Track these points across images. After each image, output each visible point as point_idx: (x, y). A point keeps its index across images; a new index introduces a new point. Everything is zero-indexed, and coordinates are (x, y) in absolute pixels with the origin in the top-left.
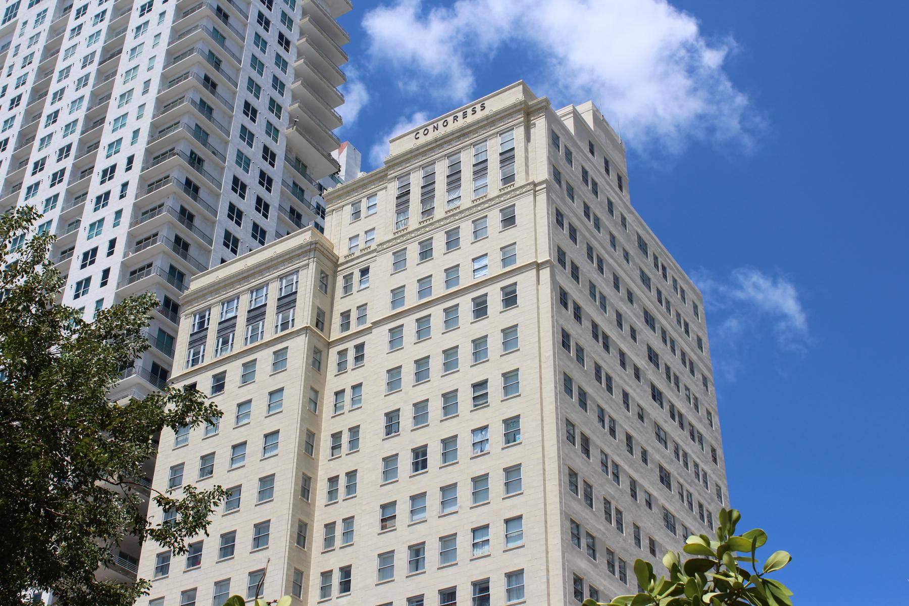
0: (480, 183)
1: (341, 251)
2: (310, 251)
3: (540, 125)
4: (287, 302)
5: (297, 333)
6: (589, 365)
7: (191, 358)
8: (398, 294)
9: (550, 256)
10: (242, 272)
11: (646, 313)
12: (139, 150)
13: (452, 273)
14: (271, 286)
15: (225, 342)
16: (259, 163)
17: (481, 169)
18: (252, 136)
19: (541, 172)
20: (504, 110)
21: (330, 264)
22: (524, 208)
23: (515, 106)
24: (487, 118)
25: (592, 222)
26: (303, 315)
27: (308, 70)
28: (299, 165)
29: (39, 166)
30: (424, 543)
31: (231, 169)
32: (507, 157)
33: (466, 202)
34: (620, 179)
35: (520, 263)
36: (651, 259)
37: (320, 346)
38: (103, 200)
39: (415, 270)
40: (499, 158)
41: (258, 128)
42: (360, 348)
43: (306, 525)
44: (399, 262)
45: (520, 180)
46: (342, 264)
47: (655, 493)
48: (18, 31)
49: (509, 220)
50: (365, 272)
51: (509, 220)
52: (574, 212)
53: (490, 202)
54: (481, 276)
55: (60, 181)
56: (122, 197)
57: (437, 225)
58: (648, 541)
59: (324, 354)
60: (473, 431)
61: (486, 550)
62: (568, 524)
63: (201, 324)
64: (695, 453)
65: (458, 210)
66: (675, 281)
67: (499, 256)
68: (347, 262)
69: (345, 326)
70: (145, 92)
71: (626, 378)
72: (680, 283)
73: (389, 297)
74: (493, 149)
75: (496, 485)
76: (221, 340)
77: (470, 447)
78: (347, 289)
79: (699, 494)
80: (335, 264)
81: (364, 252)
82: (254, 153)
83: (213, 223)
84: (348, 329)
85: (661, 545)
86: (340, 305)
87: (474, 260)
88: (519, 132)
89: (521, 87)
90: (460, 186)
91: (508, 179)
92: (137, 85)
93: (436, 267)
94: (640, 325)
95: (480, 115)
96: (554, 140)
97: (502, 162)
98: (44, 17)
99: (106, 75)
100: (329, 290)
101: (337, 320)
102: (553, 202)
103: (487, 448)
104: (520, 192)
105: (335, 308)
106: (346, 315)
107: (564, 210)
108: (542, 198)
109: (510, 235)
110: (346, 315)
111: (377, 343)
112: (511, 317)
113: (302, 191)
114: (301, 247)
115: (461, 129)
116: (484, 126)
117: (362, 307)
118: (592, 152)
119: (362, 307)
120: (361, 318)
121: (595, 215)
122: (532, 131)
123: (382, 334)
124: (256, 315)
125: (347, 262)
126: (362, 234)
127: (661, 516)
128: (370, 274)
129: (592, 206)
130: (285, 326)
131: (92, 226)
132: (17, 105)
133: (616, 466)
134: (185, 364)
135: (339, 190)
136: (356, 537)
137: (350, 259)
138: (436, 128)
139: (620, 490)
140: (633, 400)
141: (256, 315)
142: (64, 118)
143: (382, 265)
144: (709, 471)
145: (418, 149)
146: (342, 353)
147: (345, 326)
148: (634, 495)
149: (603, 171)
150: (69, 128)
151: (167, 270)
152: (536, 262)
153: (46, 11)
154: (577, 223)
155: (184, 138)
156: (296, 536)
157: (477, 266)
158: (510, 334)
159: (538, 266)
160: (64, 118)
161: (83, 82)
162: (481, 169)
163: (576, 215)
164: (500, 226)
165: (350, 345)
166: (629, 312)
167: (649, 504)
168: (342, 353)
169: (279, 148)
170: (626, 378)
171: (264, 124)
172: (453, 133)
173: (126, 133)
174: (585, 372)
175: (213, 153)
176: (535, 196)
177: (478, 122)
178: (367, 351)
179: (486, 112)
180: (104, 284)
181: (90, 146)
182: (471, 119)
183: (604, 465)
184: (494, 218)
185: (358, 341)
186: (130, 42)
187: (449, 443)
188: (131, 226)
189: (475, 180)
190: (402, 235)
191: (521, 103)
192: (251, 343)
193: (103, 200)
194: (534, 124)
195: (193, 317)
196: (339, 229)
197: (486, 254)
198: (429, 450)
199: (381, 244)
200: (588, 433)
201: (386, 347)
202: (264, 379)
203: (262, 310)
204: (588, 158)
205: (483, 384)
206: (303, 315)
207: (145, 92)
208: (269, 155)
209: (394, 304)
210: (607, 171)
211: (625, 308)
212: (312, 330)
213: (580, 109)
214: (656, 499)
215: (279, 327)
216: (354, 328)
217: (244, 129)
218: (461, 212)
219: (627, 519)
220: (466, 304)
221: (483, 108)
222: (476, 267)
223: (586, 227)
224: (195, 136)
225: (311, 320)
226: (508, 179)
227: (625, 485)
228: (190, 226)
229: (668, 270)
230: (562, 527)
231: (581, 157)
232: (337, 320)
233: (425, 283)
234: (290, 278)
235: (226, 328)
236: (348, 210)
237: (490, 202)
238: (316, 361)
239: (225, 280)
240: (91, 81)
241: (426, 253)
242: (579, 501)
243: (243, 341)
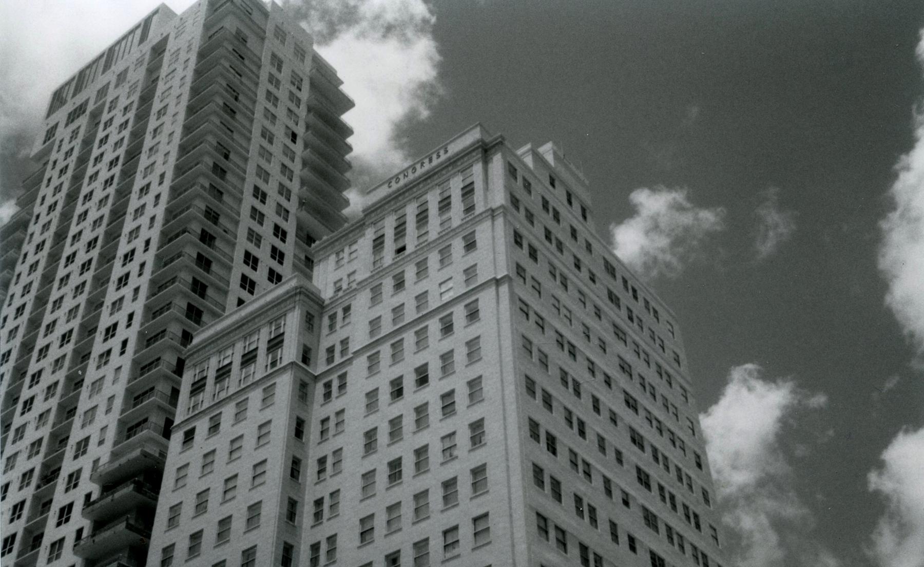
0: (445, 217)
1: (327, 294)
2: (296, 294)
3: (497, 163)
4: (276, 343)
5: (284, 368)
6: (554, 371)
8: (375, 324)
9: (508, 270)
10: (237, 322)
11: (615, 326)
12: (155, 234)
16: (269, 239)
17: (445, 205)
18: (262, 215)
19: (499, 198)
21: (316, 307)
22: (483, 233)
23: (471, 145)
24: (449, 159)
25: (554, 245)
26: (290, 352)
27: (315, 158)
29: (71, 259)
30: (399, 551)
31: (243, 244)
32: (468, 191)
33: (433, 235)
34: (584, 210)
35: (481, 280)
36: (619, 281)
37: (307, 379)
38: (123, 280)
39: (389, 300)
41: (268, 209)
42: (343, 377)
43: (292, 547)
44: (376, 293)
45: (480, 209)
46: (328, 305)
47: (632, 492)
48: (56, 148)
49: (470, 245)
50: (347, 310)
51: (470, 245)
52: (534, 235)
53: (454, 232)
54: (446, 298)
55: (88, 269)
56: (140, 275)
58: (626, 539)
59: (310, 388)
60: (443, 438)
61: (456, 552)
62: (534, 517)
64: (675, 457)
66: (647, 302)
67: (462, 278)
68: (331, 303)
69: (330, 360)
70: (161, 183)
71: (596, 385)
72: (653, 304)
73: (367, 329)
74: (456, 185)
75: (464, 488)
77: (440, 454)
78: (332, 327)
79: (683, 495)
80: (321, 305)
82: (266, 231)
83: (226, 293)
84: (333, 361)
85: (642, 543)
87: (440, 284)
88: (478, 168)
89: (478, 129)
90: (427, 222)
91: (469, 209)
92: (154, 178)
93: (407, 297)
94: (609, 338)
95: (443, 157)
96: (512, 171)
97: (463, 195)
98: (77, 133)
99: (128, 173)
101: (322, 355)
102: (511, 224)
103: (456, 453)
104: (479, 219)
106: (331, 350)
107: (523, 232)
108: (500, 221)
109: (471, 259)
110: (331, 350)
111: (357, 371)
115: (428, 172)
118: (552, 184)
119: (345, 342)
120: (344, 352)
121: (557, 239)
123: (362, 362)
124: (249, 358)
126: (345, 278)
127: (641, 514)
128: (351, 311)
129: (553, 231)
130: (274, 364)
131: (114, 304)
132: (131, 260)
133: (587, 464)
135: (325, 242)
136: (338, 555)
137: (333, 301)
139: (592, 488)
140: (604, 404)
142: (93, 216)
144: (693, 476)
145: (390, 195)
146: (328, 385)
147: (330, 360)
148: (609, 492)
149: (581, 218)
150: (97, 223)
153: (79, 128)
154: (536, 244)
156: (280, 558)
157: (443, 289)
158: (473, 346)
159: (498, 282)
160: (93, 216)
161: (108, 182)
162: (445, 205)
163: (537, 238)
164: (463, 252)
166: (599, 328)
167: (626, 503)
170: (596, 385)
171: (274, 205)
172: (420, 177)
173: (144, 220)
174: (549, 376)
175: (225, 231)
176: (493, 224)
177: (442, 164)
179: (450, 154)
180: (122, 353)
181: (113, 236)
182: (435, 162)
183: (574, 464)
184: (458, 245)
185: (340, 373)
186: (148, 142)
187: (421, 453)
188: (148, 298)
189: (440, 215)
190: (378, 272)
191: (478, 142)
193: (123, 280)
196: (325, 279)
198: (404, 462)
200: (554, 432)
201: (365, 373)
202: (255, 413)
203: (254, 353)
204: (549, 191)
205: (451, 393)
207: (161, 183)
208: (280, 232)
209: (372, 333)
210: (570, 202)
211: (592, 322)
213: (541, 150)
214: (635, 499)
216: (338, 360)
217: (254, 209)
219: (601, 515)
220: (434, 326)
221: (446, 152)
223: (548, 249)
224: (205, 216)
225: (297, 356)
226: (469, 209)
227: (598, 482)
228: (203, 295)
229: (639, 292)
230: (526, 519)
231: (541, 188)
232: (322, 355)
233: (398, 311)
234: (279, 322)
235: (224, 374)
237: (454, 232)
238: (303, 391)
239: (222, 331)
240: (116, 180)
241: (399, 285)
242: (546, 496)
243: (237, 383)
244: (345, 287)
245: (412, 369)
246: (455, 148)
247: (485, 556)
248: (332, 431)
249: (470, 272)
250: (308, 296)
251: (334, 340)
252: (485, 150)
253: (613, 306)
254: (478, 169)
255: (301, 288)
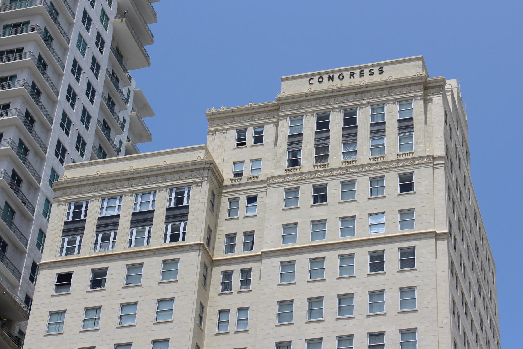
2: (204, 169)
3: (437, 100)
5: (191, 248)
7: (65, 246)
13: (348, 222)
14: (159, 195)
15: (106, 239)
20: (404, 80)
23: (415, 78)
28: (118, 53)
31: (73, 52)
32: (406, 126)
40: (397, 125)
42: (246, 273)
46: (227, 187)
50: (252, 200)
57: (333, 173)
63: (77, 214)
65: (354, 164)
68: (233, 186)
69: (230, 248)
76: (100, 236)
81: (251, 180)
86: (225, 227)
100: (215, 209)
105: (219, 228)
110: (231, 238)
112: (408, 278)
113: (117, 80)
114: (195, 163)
116: (383, 89)
117: (249, 235)
122: (429, 106)
124: (142, 219)
125: (233, 186)
128: (257, 203)
134: (59, 251)
138: (331, 79)
141: (142, 219)
143: (273, 199)
146: (227, 275)
147: (230, 248)
151: (17, 143)
152: (435, 232)
155: (41, 14)
159: (437, 236)
165: (236, 269)
168: (227, 275)
169: (107, 36)
176: (433, 169)
178: (254, 276)
179: (385, 77)
192: (136, 246)
194: (431, 100)
195: (67, 207)
197: (384, 213)
199: (272, 178)
203: (149, 216)
206: (194, 231)
208: (100, 42)
212: (204, 247)
215: (168, 238)
216: (239, 252)
218: (358, 166)
220: (362, 257)
221: (381, 72)
222: (373, 222)
236: (232, 136)
239: (107, 176)
244: (247, 173)
245: (335, 294)
246: (393, 73)
247: (241, 340)
248: (233, 325)
249: (406, 215)
250: (214, 173)
251: (238, 227)
252: (429, 87)
253: (51, 33)
254: (417, 106)
255: (211, 164)
